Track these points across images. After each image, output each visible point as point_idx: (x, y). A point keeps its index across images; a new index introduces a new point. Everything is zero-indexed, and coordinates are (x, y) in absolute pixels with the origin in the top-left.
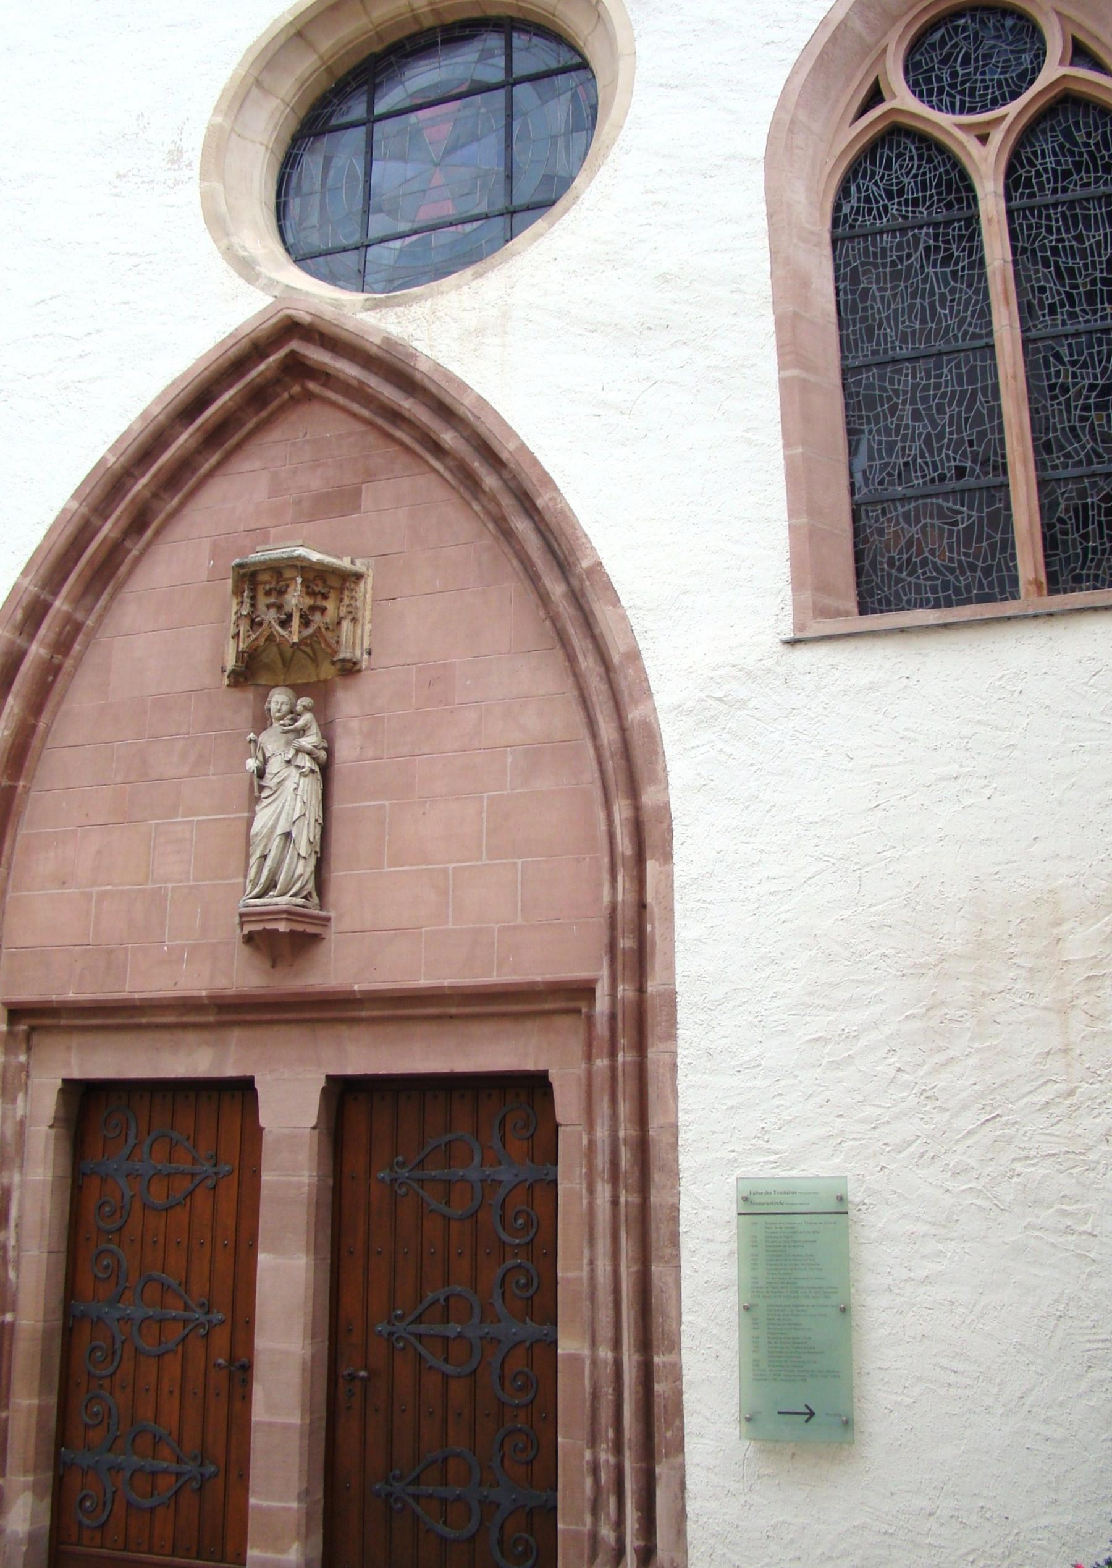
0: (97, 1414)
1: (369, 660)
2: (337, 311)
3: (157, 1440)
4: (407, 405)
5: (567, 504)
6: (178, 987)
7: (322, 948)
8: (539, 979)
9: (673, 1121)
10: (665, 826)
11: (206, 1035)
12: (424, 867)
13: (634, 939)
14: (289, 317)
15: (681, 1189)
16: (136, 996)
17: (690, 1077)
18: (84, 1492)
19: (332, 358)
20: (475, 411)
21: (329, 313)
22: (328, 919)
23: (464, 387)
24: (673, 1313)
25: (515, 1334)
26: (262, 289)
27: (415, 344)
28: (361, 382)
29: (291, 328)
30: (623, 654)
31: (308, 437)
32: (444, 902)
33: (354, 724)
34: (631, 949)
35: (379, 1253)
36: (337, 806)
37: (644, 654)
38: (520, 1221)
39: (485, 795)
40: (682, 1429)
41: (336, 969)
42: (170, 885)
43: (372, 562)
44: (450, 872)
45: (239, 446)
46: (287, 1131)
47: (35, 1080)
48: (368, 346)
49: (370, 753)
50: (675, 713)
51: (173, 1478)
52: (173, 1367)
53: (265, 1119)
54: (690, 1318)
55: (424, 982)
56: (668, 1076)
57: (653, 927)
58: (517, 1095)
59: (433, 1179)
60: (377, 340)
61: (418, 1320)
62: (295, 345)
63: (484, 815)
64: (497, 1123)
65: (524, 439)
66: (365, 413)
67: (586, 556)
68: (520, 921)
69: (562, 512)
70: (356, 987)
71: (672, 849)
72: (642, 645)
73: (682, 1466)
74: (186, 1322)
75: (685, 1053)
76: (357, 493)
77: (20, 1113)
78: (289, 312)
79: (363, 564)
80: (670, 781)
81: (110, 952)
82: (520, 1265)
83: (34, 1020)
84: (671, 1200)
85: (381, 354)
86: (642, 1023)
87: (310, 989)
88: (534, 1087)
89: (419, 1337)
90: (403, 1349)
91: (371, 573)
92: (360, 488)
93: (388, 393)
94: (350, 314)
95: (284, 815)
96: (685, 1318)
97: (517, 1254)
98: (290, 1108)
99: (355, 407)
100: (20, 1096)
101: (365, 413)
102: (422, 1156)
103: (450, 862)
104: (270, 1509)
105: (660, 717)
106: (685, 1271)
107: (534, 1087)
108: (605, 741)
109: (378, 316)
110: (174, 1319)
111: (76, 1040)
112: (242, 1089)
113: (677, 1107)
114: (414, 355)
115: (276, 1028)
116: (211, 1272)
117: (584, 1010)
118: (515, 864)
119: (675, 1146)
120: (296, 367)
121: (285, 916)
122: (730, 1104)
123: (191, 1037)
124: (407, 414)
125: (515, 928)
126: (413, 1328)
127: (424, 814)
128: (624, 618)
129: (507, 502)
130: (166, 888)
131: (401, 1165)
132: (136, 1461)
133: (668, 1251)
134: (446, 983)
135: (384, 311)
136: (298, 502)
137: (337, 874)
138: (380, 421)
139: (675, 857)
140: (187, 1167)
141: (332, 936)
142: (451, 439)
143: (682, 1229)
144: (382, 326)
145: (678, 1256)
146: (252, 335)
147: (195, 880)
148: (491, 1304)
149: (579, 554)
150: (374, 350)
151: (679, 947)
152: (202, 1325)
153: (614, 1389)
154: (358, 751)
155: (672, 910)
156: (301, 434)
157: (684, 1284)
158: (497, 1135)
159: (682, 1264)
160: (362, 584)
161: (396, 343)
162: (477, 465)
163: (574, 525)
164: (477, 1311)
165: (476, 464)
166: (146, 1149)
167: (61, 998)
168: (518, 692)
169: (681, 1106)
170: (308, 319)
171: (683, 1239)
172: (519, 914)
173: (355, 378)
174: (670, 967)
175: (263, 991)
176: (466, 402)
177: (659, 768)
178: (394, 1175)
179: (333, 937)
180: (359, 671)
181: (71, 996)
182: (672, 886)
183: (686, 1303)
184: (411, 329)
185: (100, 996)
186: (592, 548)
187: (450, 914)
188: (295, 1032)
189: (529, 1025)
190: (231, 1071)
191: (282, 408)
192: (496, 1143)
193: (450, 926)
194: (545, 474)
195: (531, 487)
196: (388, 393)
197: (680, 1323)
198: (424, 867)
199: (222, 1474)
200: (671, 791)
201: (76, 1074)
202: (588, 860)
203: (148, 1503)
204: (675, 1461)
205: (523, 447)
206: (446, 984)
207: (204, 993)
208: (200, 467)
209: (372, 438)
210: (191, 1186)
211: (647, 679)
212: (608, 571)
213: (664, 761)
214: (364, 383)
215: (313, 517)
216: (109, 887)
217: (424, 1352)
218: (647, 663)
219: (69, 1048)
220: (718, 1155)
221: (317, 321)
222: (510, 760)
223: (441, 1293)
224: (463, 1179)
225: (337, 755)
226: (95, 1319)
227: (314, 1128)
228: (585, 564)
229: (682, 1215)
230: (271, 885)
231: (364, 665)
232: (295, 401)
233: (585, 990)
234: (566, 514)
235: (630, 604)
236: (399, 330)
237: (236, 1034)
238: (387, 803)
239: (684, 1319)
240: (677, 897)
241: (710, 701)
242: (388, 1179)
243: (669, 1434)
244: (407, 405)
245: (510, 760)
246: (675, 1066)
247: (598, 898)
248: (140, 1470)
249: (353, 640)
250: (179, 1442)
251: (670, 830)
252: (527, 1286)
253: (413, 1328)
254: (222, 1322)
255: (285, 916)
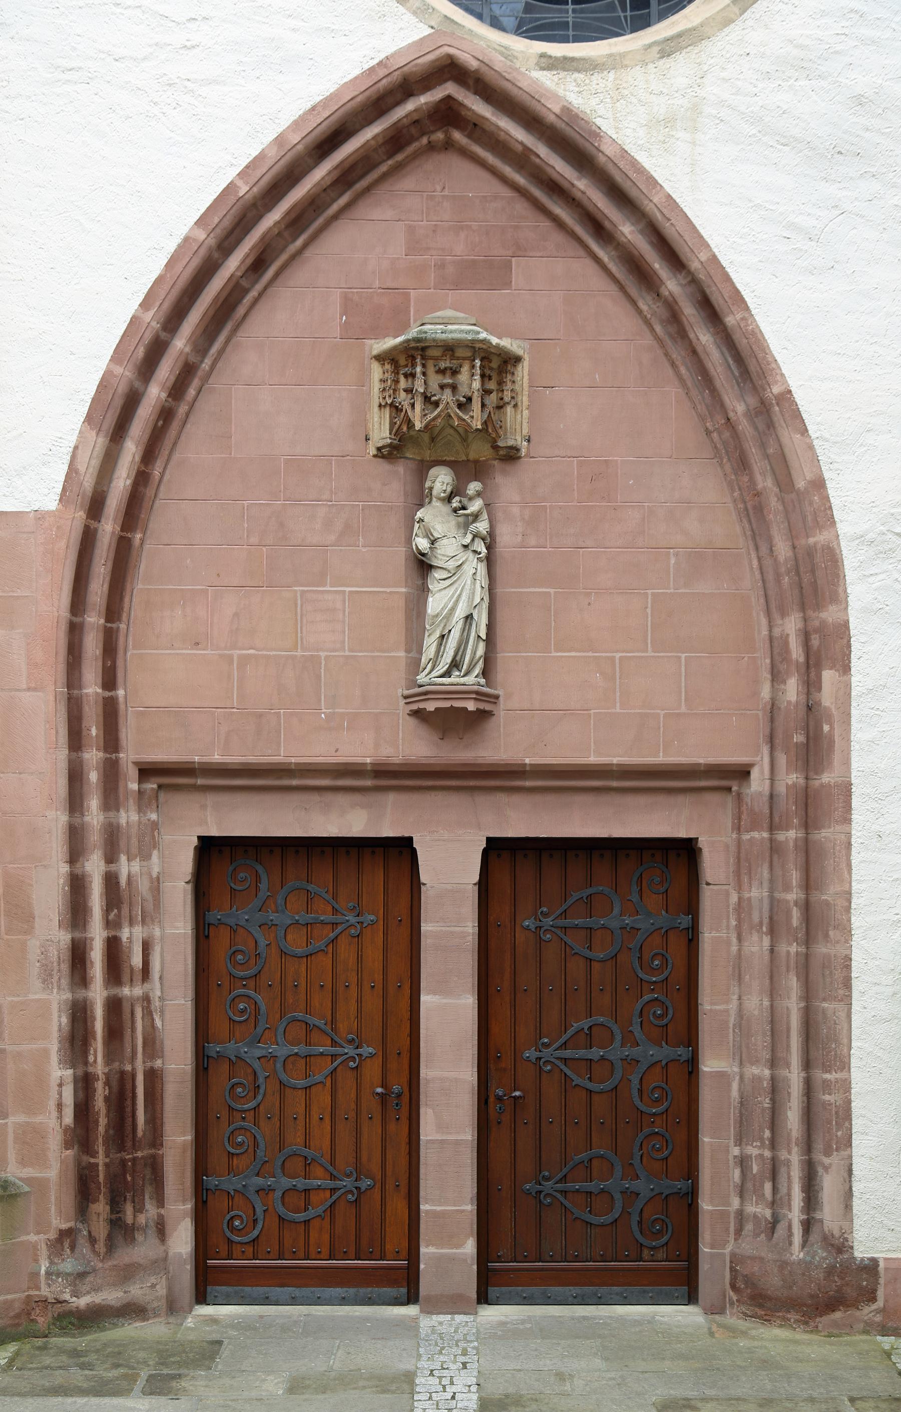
0: (241, 1144)
1: (528, 449)
2: (509, 63)
3: (307, 1163)
4: (582, 185)
5: (758, 326)
6: (338, 754)
7: (492, 723)
8: (701, 761)
9: (847, 888)
10: (845, 641)
11: (357, 797)
12: (590, 654)
13: (812, 739)
14: (450, 57)
15: (853, 943)
16: (293, 760)
17: (862, 854)
18: (232, 1213)
19: (493, 114)
20: (665, 211)
21: (499, 63)
22: (497, 697)
23: (653, 182)
24: (845, 1041)
25: (652, 1055)
26: (415, 13)
27: (599, 122)
28: (526, 149)
29: (450, 69)
30: (809, 482)
31: (446, 193)
32: (610, 694)
33: (515, 510)
34: (802, 742)
35: (526, 990)
36: (499, 590)
37: (829, 485)
38: (656, 962)
39: (649, 592)
40: (851, 1129)
41: (502, 745)
42: (323, 654)
43: (526, 345)
44: (617, 661)
45: (368, 189)
46: (449, 887)
47: (166, 837)
48: (543, 112)
49: (533, 541)
50: (857, 542)
51: (328, 1193)
52: (323, 1098)
53: (425, 876)
54: (859, 1044)
55: (593, 759)
56: (844, 852)
57: (832, 728)
58: (653, 855)
59: (576, 927)
60: (557, 109)
61: (564, 1046)
62: (450, 89)
63: (649, 611)
64: (635, 879)
65: (715, 250)
66: (520, 180)
67: (776, 382)
68: (683, 709)
69: (753, 333)
70: (527, 761)
71: (850, 662)
72: (827, 475)
73: (850, 1157)
74: (334, 1057)
75: (859, 834)
76: (508, 266)
77: (155, 871)
78: (452, 51)
79: (519, 347)
80: (850, 603)
81: (261, 715)
82: (656, 999)
83: (168, 778)
84: (847, 952)
85: (560, 125)
86: (815, 808)
87: (480, 761)
88: (685, 851)
89: (565, 1060)
90: (550, 1071)
91: (526, 357)
92: (510, 262)
93: (560, 167)
94: (523, 70)
95: (464, 597)
96: (854, 1044)
97: (653, 989)
98: (450, 866)
99: (508, 171)
100: (155, 853)
101: (520, 180)
102: (564, 907)
103: (617, 651)
104: (443, 1214)
105: (842, 544)
106: (856, 1007)
107: (685, 851)
108: (781, 559)
109: (556, 78)
110: (322, 1054)
111: (211, 799)
112: (401, 850)
113: (851, 877)
114: (597, 134)
115: (433, 793)
116: (359, 1010)
117: (734, 788)
118: (680, 657)
119: (848, 909)
120: (448, 114)
121: (474, 696)
122: (895, 877)
123: (342, 799)
124: (578, 195)
125: (678, 715)
126: (559, 1053)
127: (589, 604)
128: (811, 447)
129: (689, 311)
130: (320, 657)
131: (545, 915)
132: (286, 1182)
133: (841, 992)
134: (615, 761)
135: (563, 74)
136: (441, 266)
137: (505, 656)
138: (537, 193)
139: (853, 669)
140: (327, 917)
141: (501, 711)
142: (632, 233)
143: (853, 975)
144: (561, 92)
145: (850, 996)
146: (405, 69)
147: (351, 650)
148: (630, 1031)
149: (770, 379)
150: (551, 118)
151: (855, 746)
152: (353, 1059)
153: (771, 1099)
154: (520, 538)
155: (849, 715)
156: (439, 188)
157: (854, 1017)
158: (635, 888)
159: (853, 1003)
160: (519, 368)
161: (577, 116)
162: (658, 265)
163: (765, 348)
164: (618, 1038)
165: (657, 266)
166: (280, 901)
167: (206, 759)
168: (685, 497)
169: (854, 877)
170: (474, 64)
171: (854, 983)
172: (683, 703)
173: (521, 143)
174: (847, 763)
175: (432, 761)
176: (656, 200)
177: (840, 590)
178: (538, 924)
179: (502, 713)
180: (520, 458)
181: (217, 757)
182: (850, 695)
183: (855, 1032)
184: (594, 102)
185: (251, 759)
186: (782, 375)
187: (618, 698)
188: (454, 799)
189: (680, 799)
190: (388, 831)
191: (415, 156)
192: (635, 898)
193: (618, 710)
194: (738, 292)
195: (721, 302)
196: (560, 167)
197: (850, 1048)
198: (590, 654)
199: (378, 1185)
200: (850, 611)
201: (214, 831)
202: (746, 659)
203: (301, 1216)
204: (845, 1153)
205: (714, 259)
206: (615, 762)
207: (368, 760)
208: (602, 248)
209: (521, 207)
210: (332, 935)
211: (830, 508)
212: (797, 400)
213: (845, 584)
214: (531, 150)
215: (458, 285)
216: (252, 651)
217: (569, 1072)
218: (831, 492)
219: (203, 807)
220: (885, 917)
221: (484, 69)
222: (673, 561)
223: (585, 1024)
224: (604, 927)
225: (498, 539)
226: (234, 1059)
227: (475, 884)
228: (776, 390)
229: (854, 964)
230: (455, 664)
231: (523, 452)
232: (432, 147)
233: (743, 773)
234: (757, 337)
235: (817, 435)
236: (580, 101)
237: (391, 797)
238: (552, 591)
239: (853, 1044)
240: (854, 704)
241: (890, 536)
242: (532, 927)
243: (839, 1133)
244: (582, 185)
245: (673, 561)
246: (849, 844)
247: (756, 694)
248: (294, 1189)
249: (517, 426)
250: (332, 1163)
251: (849, 646)
252: (661, 1017)
253: (559, 1053)
254: (372, 1056)
255: (474, 696)
